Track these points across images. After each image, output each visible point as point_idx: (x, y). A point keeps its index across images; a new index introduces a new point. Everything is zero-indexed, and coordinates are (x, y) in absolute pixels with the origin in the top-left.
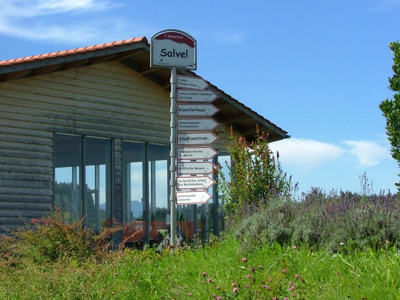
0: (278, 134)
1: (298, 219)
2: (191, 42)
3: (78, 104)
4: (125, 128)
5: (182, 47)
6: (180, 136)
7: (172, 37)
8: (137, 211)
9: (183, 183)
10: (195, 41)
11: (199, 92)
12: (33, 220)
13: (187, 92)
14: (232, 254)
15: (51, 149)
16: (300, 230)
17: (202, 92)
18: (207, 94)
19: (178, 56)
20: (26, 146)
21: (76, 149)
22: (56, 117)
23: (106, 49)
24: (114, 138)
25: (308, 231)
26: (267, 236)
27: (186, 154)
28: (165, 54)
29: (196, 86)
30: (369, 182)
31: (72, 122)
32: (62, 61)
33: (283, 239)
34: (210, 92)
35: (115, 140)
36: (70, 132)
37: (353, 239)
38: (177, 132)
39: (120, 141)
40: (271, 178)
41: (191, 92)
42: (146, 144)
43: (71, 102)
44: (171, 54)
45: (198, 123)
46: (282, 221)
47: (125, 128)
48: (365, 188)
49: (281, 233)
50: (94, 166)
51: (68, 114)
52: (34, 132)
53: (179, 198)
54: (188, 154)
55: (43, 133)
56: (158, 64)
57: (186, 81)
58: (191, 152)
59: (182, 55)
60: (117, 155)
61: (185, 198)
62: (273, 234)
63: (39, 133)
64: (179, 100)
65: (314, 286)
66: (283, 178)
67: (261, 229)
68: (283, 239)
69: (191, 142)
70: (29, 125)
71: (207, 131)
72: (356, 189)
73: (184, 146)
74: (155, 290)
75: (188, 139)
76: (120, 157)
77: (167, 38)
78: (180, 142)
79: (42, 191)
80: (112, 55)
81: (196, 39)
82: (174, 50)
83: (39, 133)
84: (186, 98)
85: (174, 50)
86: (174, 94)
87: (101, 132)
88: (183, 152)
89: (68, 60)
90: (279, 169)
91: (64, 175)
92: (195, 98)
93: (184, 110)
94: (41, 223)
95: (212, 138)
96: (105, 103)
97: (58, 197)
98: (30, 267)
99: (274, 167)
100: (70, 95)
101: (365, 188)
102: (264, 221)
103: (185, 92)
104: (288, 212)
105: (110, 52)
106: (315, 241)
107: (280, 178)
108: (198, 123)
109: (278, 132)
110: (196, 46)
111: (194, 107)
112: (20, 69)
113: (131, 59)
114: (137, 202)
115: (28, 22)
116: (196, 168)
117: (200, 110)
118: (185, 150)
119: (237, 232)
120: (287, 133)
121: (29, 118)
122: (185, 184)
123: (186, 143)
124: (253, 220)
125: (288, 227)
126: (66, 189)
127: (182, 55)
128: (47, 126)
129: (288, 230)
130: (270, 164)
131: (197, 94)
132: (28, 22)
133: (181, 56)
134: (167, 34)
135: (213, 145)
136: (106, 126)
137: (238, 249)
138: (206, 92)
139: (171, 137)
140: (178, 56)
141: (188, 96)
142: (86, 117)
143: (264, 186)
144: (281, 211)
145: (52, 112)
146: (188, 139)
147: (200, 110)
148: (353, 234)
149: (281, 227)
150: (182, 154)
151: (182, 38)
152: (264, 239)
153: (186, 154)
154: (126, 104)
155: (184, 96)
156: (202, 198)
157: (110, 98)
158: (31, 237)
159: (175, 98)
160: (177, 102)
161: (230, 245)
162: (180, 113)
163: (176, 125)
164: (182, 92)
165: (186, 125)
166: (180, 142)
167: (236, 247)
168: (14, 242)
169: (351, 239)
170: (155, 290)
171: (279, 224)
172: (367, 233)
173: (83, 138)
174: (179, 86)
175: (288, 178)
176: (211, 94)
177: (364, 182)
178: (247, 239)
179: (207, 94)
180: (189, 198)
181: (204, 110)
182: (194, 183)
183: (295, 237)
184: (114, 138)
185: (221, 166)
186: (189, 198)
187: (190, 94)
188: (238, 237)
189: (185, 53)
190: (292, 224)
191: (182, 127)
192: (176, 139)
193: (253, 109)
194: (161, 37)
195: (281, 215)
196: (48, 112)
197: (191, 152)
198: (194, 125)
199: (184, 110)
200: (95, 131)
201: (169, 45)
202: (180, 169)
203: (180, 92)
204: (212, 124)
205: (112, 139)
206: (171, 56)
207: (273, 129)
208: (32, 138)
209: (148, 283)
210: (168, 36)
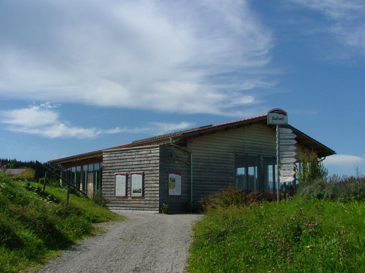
0: (331, 152)
1: (327, 188)
2: (284, 114)
3: (245, 141)
4: (265, 151)
5: (281, 116)
6: (280, 153)
7: (277, 112)
8: (271, 186)
9: (282, 173)
10: (287, 113)
11: (289, 134)
12: (221, 189)
13: (284, 135)
14: (298, 203)
15: (234, 160)
16: (327, 193)
17: (290, 134)
18: (292, 135)
19: (279, 119)
20: (224, 159)
21: (244, 161)
22: (236, 147)
23: (256, 118)
24: (260, 155)
25: (330, 193)
26: (313, 195)
27: (283, 161)
28: (274, 119)
29: (288, 132)
30: (359, 171)
31: (242, 149)
32: (237, 124)
33: (320, 197)
34: (293, 134)
35: (261, 156)
36: (241, 153)
37: (349, 197)
38: (279, 152)
39: (263, 156)
40: (319, 171)
41: (285, 134)
42: (259, 156)
43: (242, 141)
44: (276, 119)
45: (288, 148)
46: (320, 189)
47: (265, 151)
48: (357, 174)
49: (319, 194)
50: (253, 167)
51: (240, 146)
52: (227, 153)
53: (280, 180)
54: (285, 161)
55: (230, 154)
56: (271, 123)
57: (283, 130)
58: (285, 160)
59: (281, 119)
60: (261, 162)
61: (283, 179)
62: (315, 195)
63: (229, 154)
64: (280, 138)
65: (330, 217)
66: (325, 171)
67: (311, 192)
68: (320, 197)
69: (285, 156)
70: (225, 150)
71: (292, 151)
72: (355, 176)
73: (283, 157)
74: (265, 218)
75: (284, 154)
76: (263, 163)
77: (274, 112)
78: (281, 156)
79: (230, 178)
80: (258, 121)
81: (287, 112)
82: (277, 117)
83: (229, 154)
84: (283, 137)
85: (277, 117)
86: (278, 135)
87: (255, 153)
88: (282, 160)
89: (240, 124)
90: (323, 167)
91: (241, 171)
92: (287, 137)
93: (282, 142)
94: (225, 190)
95: (294, 154)
96: (256, 141)
97: (237, 180)
98: (219, 209)
99: (320, 166)
100: (241, 138)
101: (357, 174)
102: (312, 189)
103: (282, 134)
104: (323, 186)
105: (258, 120)
106: (333, 197)
107: (323, 171)
108: (288, 148)
109: (331, 151)
110: (287, 115)
111: (286, 141)
112: (220, 128)
113: (261, 121)
114: (271, 182)
115: (228, 110)
116: (288, 167)
117: (289, 142)
118: (283, 159)
119: (301, 194)
120: (335, 152)
121: (225, 148)
122: (283, 174)
123: (283, 156)
124: (307, 189)
125: (323, 191)
126: (241, 177)
127: (281, 119)
128: (232, 151)
129: (322, 193)
130: (319, 164)
131: (288, 135)
132: (228, 110)
133: (281, 119)
134: (275, 110)
135: (295, 157)
136: (256, 150)
137: (301, 201)
138: (292, 134)
139: (277, 154)
140: (279, 119)
141: (284, 136)
142: (248, 147)
143: (316, 173)
144: (320, 185)
145: (234, 145)
146: (284, 154)
147: (289, 142)
148: (348, 194)
149: (319, 191)
150: (282, 161)
151: (281, 112)
152: (312, 197)
153: (283, 161)
154: (265, 141)
155: (282, 136)
156: (290, 179)
157: (252, 139)
158: (220, 196)
159: (279, 137)
160: (279, 139)
161: (299, 199)
162: (281, 144)
163: (279, 149)
164: (281, 134)
165: (283, 148)
166: (281, 156)
167: (49, 170)
168: (214, 198)
169: (348, 197)
170: (265, 218)
171: (318, 190)
172: (355, 194)
173: (247, 155)
174: (280, 132)
175: (326, 170)
176: (293, 135)
177: (357, 172)
178: (305, 197)
179: (292, 135)
180: (285, 179)
181: (291, 142)
182: (287, 173)
183: (325, 196)
184: (260, 155)
185: (297, 166)
186: (285, 179)
187: (285, 135)
188: (301, 196)
189: (282, 118)
190: (324, 190)
191: (281, 149)
192: (279, 155)
193: (317, 140)
194: (272, 112)
195: (319, 186)
196: (233, 145)
197: (285, 160)
198: (287, 148)
199: (282, 142)
200: (252, 152)
201: (276, 115)
202: (281, 167)
203: (280, 135)
204: (294, 148)
205: (260, 156)
206: (276, 120)
207: (329, 150)
208: (226, 156)
209: (262, 215)
210: (275, 111)
